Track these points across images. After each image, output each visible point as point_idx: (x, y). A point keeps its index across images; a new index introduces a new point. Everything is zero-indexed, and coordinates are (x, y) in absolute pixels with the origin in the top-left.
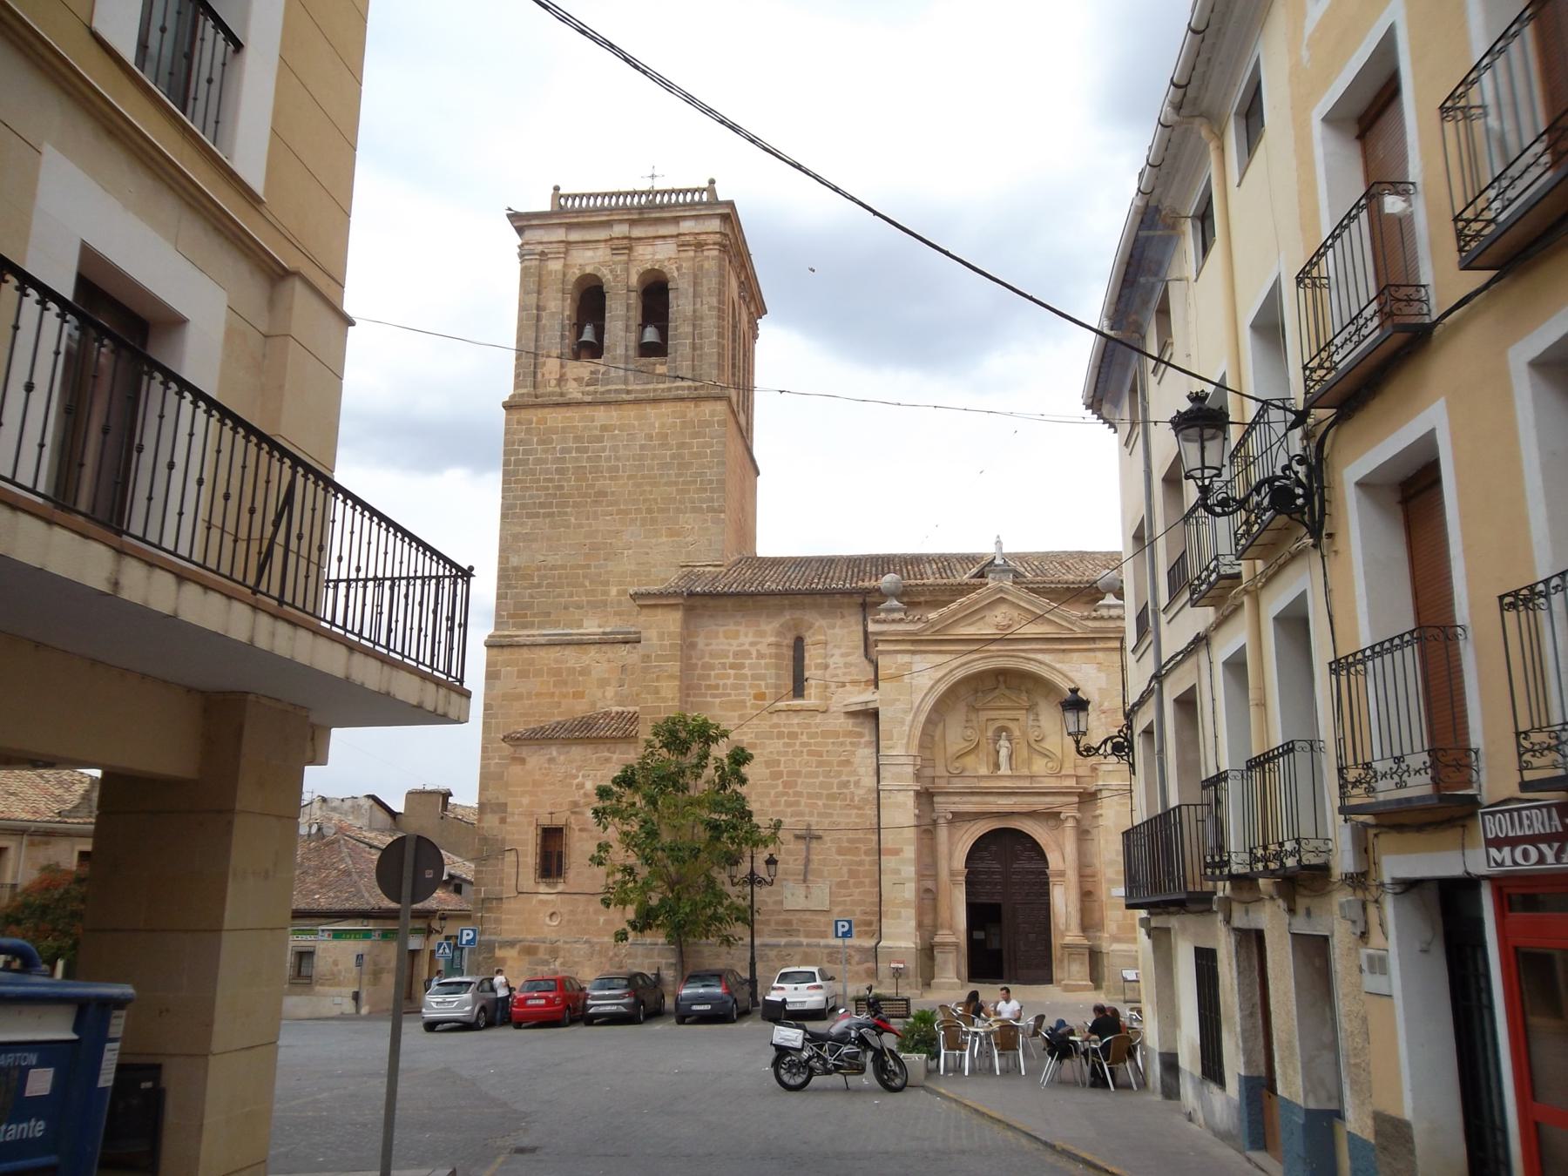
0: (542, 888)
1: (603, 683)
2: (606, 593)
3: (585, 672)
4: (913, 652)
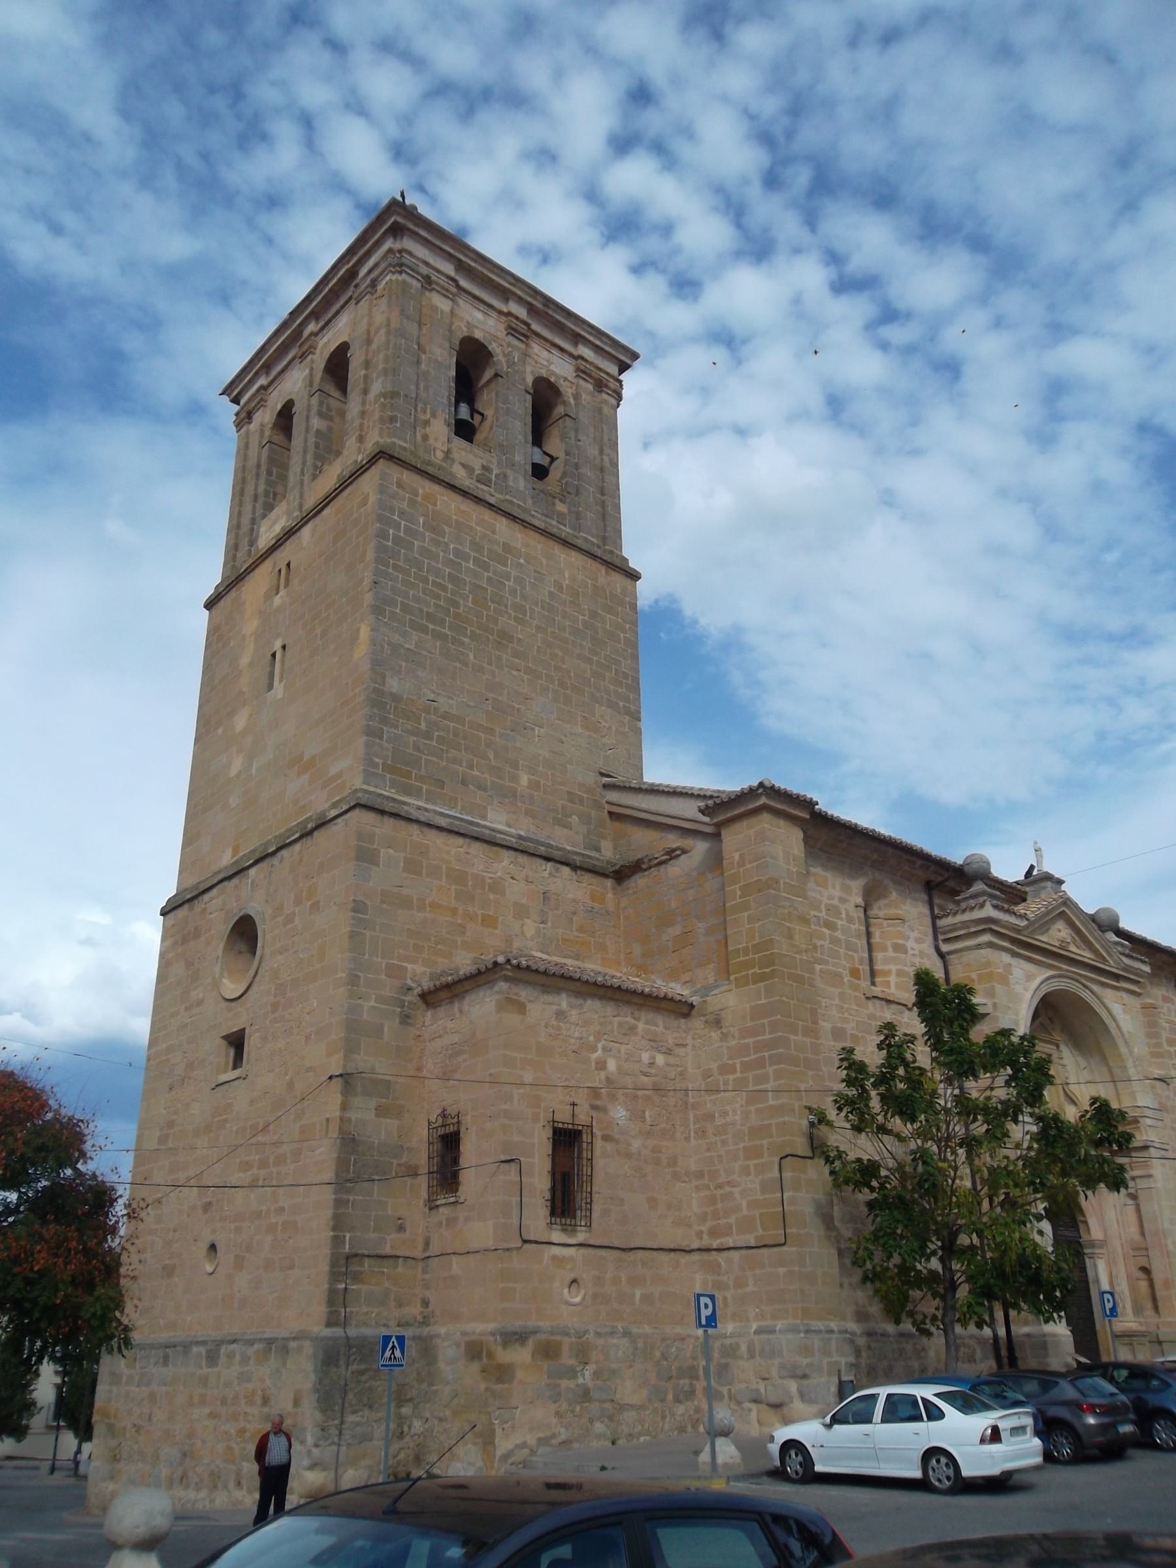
0: (557, 1236)
1: (521, 912)
2: (514, 778)
3: (496, 887)
4: (1015, 955)
